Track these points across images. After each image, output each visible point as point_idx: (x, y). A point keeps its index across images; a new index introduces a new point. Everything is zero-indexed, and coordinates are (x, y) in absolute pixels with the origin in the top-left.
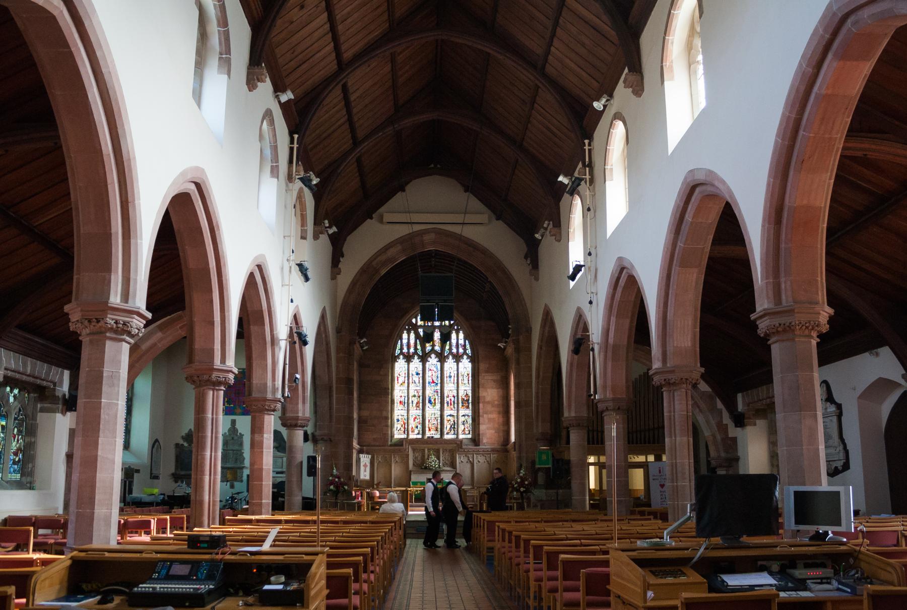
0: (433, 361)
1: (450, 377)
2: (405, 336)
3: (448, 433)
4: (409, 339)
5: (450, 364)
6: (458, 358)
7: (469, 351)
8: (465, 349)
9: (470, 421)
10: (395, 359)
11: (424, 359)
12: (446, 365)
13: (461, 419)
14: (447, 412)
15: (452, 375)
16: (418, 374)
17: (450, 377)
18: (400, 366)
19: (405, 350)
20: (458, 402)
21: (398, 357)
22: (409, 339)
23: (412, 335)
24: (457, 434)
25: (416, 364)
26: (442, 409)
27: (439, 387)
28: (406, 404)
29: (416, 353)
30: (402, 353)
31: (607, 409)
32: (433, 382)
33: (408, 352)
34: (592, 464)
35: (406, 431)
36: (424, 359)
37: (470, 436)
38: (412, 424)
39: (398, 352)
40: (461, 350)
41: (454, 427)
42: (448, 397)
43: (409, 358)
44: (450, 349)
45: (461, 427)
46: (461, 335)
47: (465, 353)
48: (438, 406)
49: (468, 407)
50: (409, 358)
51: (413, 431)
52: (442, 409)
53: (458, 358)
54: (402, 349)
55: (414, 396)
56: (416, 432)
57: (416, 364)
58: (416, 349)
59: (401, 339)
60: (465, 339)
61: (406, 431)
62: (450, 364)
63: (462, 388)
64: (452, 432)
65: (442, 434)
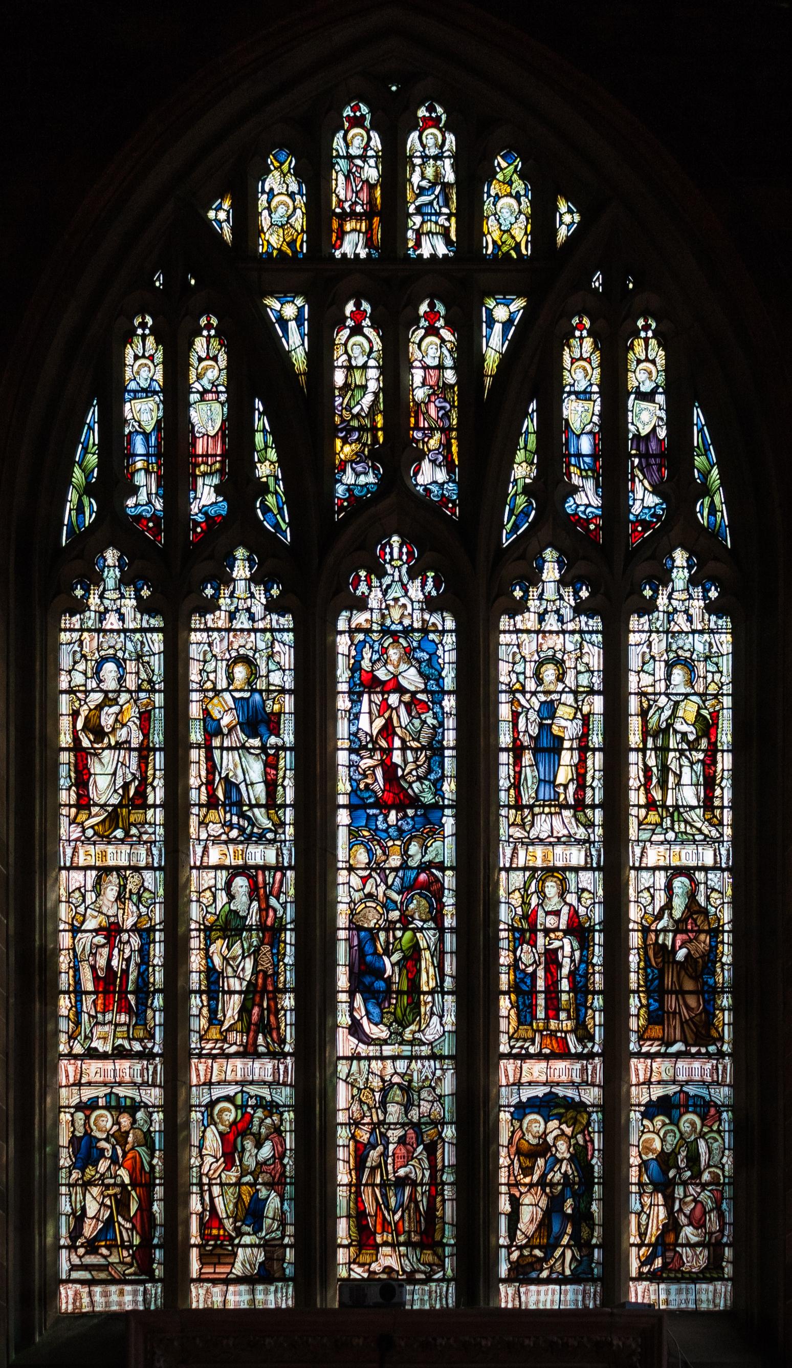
0: (397, 593)
1: (548, 747)
2: (142, 364)
3: (523, 1273)
4: (175, 394)
5: (544, 639)
6: (614, 580)
7: (713, 510)
8: (679, 490)
9: (717, 1153)
10: (51, 582)
11: (312, 587)
12: (518, 646)
13: (646, 1139)
14: (526, 1075)
15: (566, 725)
16: (257, 721)
17: (548, 747)
18: (101, 645)
19: (145, 496)
20: (626, 983)
21: (87, 544)
22: (175, 394)
23: (209, 364)
24: (613, 1277)
25: (242, 637)
26: (474, 1052)
27: (445, 849)
28: (155, 1002)
29: (239, 520)
30: (115, 526)
31: (101, 681)
32: (397, 795)
33: (393, 128)
34: (344, 806)
35: (160, 1250)
36: (312, 587)
37: (713, 1296)
38: (213, 1178)
39: (78, 509)
40: (643, 499)
41: (586, 1207)
42: (526, 931)
43: (176, 578)
44: (550, 486)
45: (647, 1215)
46: (647, 366)
47: (677, 523)
48: (439, 1025)
49: (701, 1034)
50: (176, 578)
51: (218, 1251)
52: (474, 1052)
53: (614, 580)
54: (113, 483)
55: (229, 927)
56: (246, 1258)
57: (242, 637)
58: (239, 484)
59: (112, 392)
60: (678, 393)
61: (160, 1250)
62: (544, 639)
63: (652, 853)
64: (566, 1258)
65: (475, 1274)
